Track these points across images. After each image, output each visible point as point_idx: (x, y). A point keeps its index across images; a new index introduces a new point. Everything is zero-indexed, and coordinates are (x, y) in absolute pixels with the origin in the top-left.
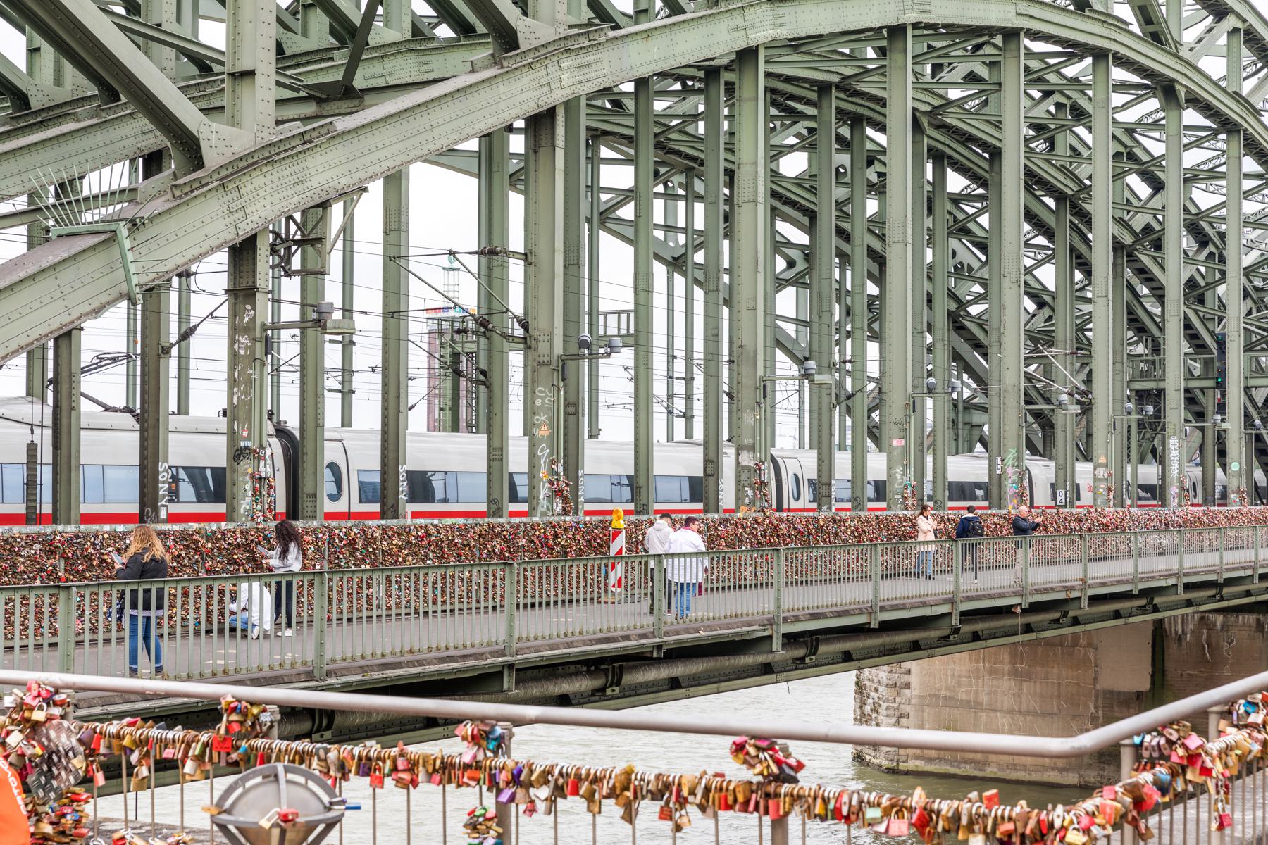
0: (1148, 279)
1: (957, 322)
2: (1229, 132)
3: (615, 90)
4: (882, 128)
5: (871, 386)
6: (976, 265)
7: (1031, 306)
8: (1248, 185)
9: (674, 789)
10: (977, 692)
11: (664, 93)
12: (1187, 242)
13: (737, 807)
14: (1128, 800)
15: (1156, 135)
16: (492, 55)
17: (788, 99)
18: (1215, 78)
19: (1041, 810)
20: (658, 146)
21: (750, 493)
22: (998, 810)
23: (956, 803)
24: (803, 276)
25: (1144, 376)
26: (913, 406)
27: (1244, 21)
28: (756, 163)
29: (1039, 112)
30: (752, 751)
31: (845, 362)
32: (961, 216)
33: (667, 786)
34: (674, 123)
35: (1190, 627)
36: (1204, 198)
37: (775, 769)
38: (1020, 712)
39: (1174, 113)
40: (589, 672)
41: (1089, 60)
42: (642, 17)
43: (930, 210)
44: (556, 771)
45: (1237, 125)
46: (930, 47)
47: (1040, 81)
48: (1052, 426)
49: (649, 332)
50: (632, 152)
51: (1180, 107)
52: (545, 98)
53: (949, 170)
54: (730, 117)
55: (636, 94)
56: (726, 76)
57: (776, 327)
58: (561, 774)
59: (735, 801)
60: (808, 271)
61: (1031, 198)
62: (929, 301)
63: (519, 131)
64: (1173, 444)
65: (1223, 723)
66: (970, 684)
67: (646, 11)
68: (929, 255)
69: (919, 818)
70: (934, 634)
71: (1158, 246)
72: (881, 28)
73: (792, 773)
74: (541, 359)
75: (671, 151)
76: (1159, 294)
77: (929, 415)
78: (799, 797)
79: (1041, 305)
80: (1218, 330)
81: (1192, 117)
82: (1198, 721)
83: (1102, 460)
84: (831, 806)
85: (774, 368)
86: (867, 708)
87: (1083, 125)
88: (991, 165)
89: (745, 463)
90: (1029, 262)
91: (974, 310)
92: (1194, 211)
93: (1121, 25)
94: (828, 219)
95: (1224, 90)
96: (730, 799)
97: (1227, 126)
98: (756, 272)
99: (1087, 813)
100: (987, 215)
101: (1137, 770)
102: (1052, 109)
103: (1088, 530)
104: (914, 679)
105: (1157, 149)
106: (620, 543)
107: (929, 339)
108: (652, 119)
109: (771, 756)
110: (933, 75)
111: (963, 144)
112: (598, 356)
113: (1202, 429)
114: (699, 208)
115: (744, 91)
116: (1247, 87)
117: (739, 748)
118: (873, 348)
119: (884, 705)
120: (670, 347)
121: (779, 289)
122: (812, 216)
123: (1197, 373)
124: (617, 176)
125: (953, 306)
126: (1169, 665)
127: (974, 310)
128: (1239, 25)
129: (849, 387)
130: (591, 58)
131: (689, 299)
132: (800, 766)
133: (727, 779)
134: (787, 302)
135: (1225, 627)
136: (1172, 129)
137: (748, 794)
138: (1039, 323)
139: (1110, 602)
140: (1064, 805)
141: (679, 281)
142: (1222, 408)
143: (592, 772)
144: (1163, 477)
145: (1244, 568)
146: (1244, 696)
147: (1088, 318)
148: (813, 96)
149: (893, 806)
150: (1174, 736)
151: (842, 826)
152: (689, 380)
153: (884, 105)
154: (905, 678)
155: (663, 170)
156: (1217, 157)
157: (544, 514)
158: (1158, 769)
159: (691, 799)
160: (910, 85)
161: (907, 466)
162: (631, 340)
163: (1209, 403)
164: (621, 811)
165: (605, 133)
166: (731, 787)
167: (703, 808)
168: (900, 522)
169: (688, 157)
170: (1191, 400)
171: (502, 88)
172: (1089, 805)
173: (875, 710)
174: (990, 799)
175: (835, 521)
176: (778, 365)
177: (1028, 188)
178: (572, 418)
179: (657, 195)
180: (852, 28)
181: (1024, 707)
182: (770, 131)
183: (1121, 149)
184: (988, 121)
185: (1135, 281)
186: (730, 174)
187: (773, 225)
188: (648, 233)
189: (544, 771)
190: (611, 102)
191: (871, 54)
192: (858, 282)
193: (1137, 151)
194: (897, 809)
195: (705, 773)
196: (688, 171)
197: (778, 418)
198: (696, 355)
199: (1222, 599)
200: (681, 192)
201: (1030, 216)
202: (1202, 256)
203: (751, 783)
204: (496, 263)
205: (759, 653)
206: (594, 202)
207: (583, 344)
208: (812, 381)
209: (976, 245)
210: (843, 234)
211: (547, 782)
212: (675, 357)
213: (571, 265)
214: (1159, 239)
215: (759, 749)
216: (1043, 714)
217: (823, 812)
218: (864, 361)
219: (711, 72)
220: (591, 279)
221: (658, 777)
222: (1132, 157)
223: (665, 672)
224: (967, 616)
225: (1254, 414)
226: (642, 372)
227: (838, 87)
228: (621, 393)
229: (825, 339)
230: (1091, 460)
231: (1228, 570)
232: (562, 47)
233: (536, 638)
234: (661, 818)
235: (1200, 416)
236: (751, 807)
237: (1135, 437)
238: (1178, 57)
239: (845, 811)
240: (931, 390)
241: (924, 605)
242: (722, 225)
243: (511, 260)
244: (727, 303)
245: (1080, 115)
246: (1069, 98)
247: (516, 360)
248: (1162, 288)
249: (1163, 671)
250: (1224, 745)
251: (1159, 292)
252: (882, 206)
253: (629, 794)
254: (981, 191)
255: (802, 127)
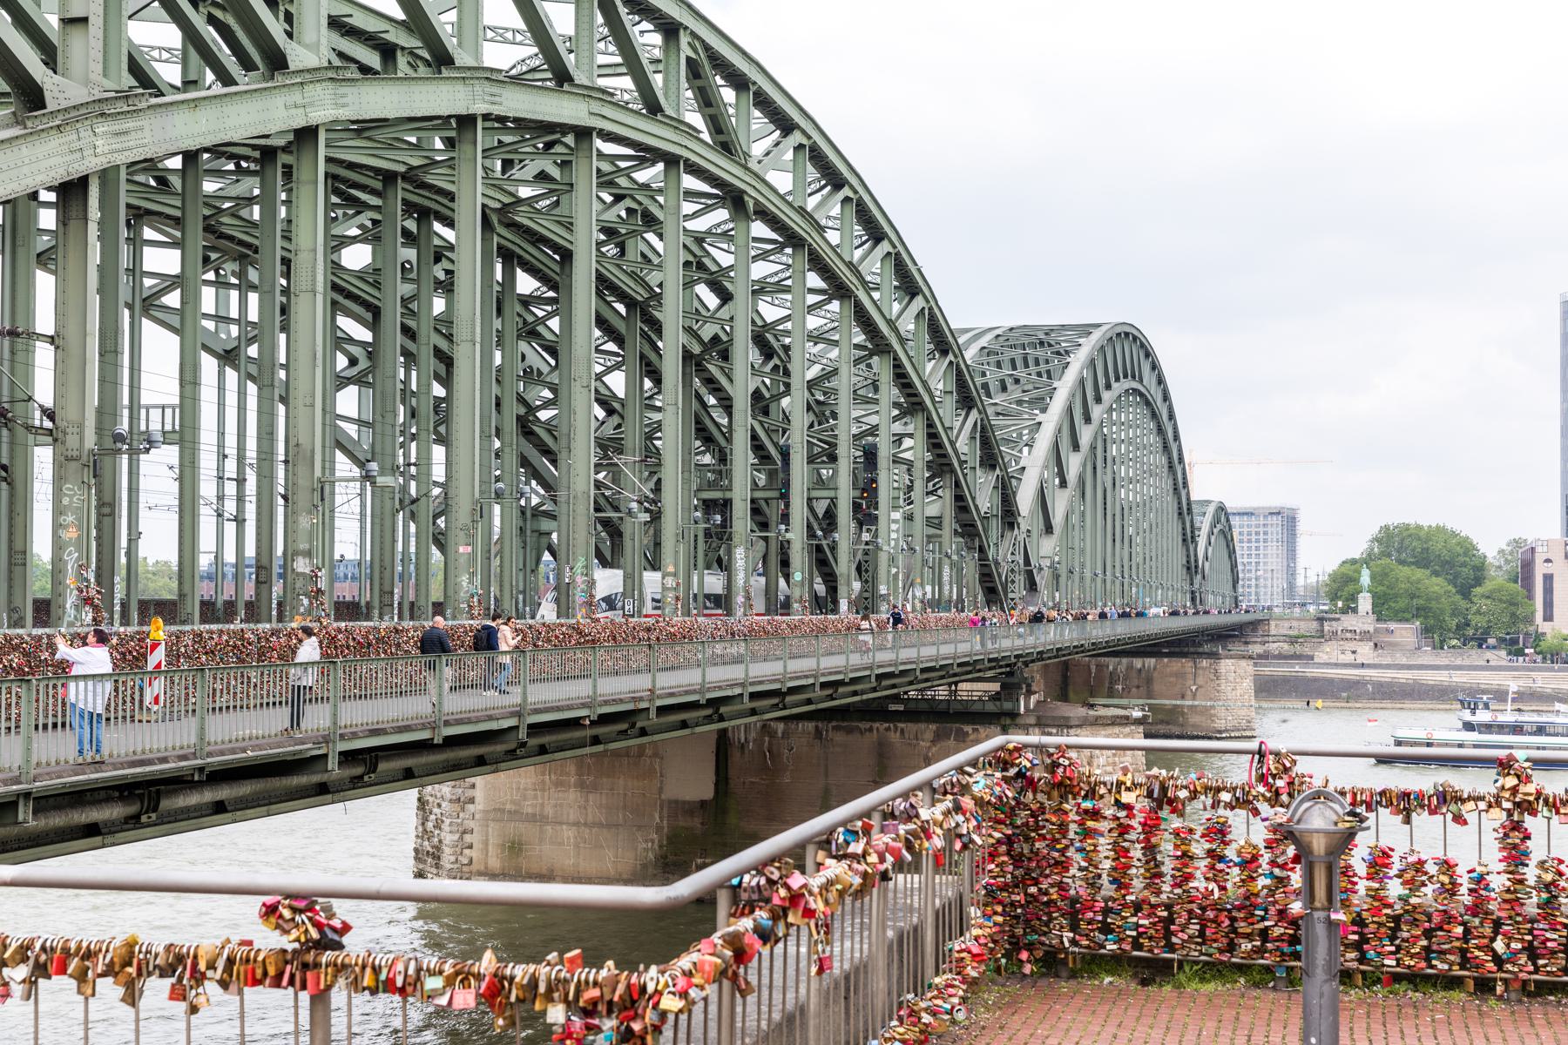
0: (716, 389)
1: (526, 426)
2: (794, 247)
3: (160, 166)
4: (450, 223)
5: (436, 491)
6: (545, 369)
7: (600, 413)
8: (812, 299)
9: (189, 962)
10: (542, 805)
11: (218, 173)
12: (754, 355)
13: (268, 982)
14: (729, 953)
15: (725, 246)
16: (14, 113)
17: (351, 187)
18: (782, 192)
19: (631, 972)
20: (208, 229)
21: (306, 602)
22: (582, 974)
23: (532, 968)
24: (366, 375)
25: (711, 485)
26: (481, 512)
27: (809, 138)
28: (315, 250)
29: (610, 216)
30: (287, 914)
31: (409, 465)
32: (530, 319)
33: (180, 959)
34: (227, 205)
35: (753, 735)
36: (770, 311)
37: (315, 934)
38: (585, 824)
39: (742, 225)
40: (122, 798)
41: (660, 166)
42: (192, 87)
43: (499, 312)
44: (38, 946)
45: (802, 239)
46: (500, 141)
47: (611, 184)
48: (620, 535)
49: (195, 429)
50: (178, 234)
51: (748, 219)
52: (76, 166)
53: (519, 271)
54: (288, 202)
55: (183, 172)
56: (284, 158)
57: (336, 426)
58: (43, 948)
59: (265, 974)
60: (371, 370)
61: (601, 303)
62: (498, 405)
63: (47, 205)
64: (739, 554)
65: (821, 855)
66: (535, 797)
67: (195, 82)
68: (498, 358)
69: (488, 988)
70: (500, 748)
71: (725, 356)
72: (450, 117)
73: (336, 937)
74: (69, 453)
75: (222, 236)
76: (727, 405)
77: (497, 521)
78: (344, 966)
79: (610, 412)
80: (782, 442)
81: (759, 229)
82: (796, 857)
83: (671, 569)
84: (383, 977)
85: (333, 470)
86: (430, 825)
87: (654, 232)
88: (562, 268)
89: (300, 570)
90: (599, 369)
91: (544, 415)
92: (760, 323)
93: (692, 132)
94: (393, 316)
95: (790, 204)
96: (259, 972)
97: (793, 240)
98: (314, 366)
99: (684, 973)
100: (557, 318)
101: (733, 915)
102: (623, 214)
103: (653, 640)
104: (478, 794)
105: (726, 260)
106: (159, 655)
107: (497, 444)
108: (201, 200)
109: (310, 919)
110: (504, 171)
111: (533, 244)
112: (139, 452)
113: (766, 539)
114: (253, 298)
115: (302, 173)
116: (811, 203)
117: (270, 911)
118: (439, 452)
119: (447, 821)
120: (221, 445)
121: (339, 387)
122: (376, 312)
123: (761, 483)
124: (162, 260)
125: (522, 411)
126: (732, 772)
127: (544, 415)
128: (805, 141)
129: (413, 492)
130: (129, 124)
131: (242, 394)
132: (347, 927)
133: (256, 947)
134: (348, 401)
135: (786, 734)
136: (740, 240)
137: (281, 965)
138: (608, 430)
139: (679, 712)
140: (657, 964)
141: (231, 376)
142: (785, 518)
143: (84, 945)
144: (729, 586)
145: (806, 677)
146: (843, 823)
147: (659, 426)
148: (378, 185)
149: (457, 974)
150: (776, 876)
151: (397, 998)
152: (241, 481)
153: (453, 200)
154: (469, 793)
155: (213, 256)
156: (782, 271)
157: (71, 624)
158: (758, 913)
159: (210, 974)
160: (479, 181)
161: (472, 575)
162: (177, 436)
163: (773, 513)
164: (121, 991)
165: (149, 212)
166: (260, 958)
167: (224, 984)
168: (466, 632)
169: (241, 243)
170: (756, 511)
171: (25, 151)
172: (685, 962)
173: (438, 826)
174: (572, 961)
175: (397, 631)
176: (338, 466)
177: (599, 294)
178: (107, 520)
179: (207, 283)
180: (420, 115)
181: (590, 819)
182: (330, 221)
183: (691, 259)
184: (559, 222)
185: (703, 391)
186: (286, 262)
187: (333, 320)
188: (196, 323)
189: (21, 946)
190: (156, 178)
191: (439, 145)
192: (424, 381)
193: (706, 261)
194: (463, 977)
195: (228, 941)
196: (242, 259)
197: (337, 523)
198: (248, 454)
199: (785, 708)
200: (234, 281)
201: (601, 322)
202: (768, 368)
203: (284, 951)
204: (20, 347)
205: (314, 773)
206: (136, 286)
207: (119, 438)
208: (373, 484)
209: (546, 348)
210: (407, 331)
211: (25, 959)
212: (225, 456)
213: (109, 351)
214: (727, 350)
215: (294, 910)
216: (609, 826)
217: (372, 984)
218: (429, 464)
219: (268, 154)
220: (132, 369)
221: (169, 948)
222: (701, 266)
223: (209, 796)
224: (535, 729)
225: (816, 526)
226: (188, 471)
227: (405, 177)
228: (166, 493)
229: (388, 440)
230: (659, 569)
231: (791, 679)
232: (97, 110)
233: (58, 763)
234: (171, 998)
235: (764, 526)
236: (285, 982)
237: (701, 546)
238: (747, 169)
239: (399, 982)
240: (499, 495)
241: (490, 718)
242: (278, 318)
243: (38, 344)
244: (284, 400)
245: (650, 221)
246: (640, 204)
247: (43, 458)
248: (729, 399)
249: (727, 779)
250: (824, 880)
251: (727, 403)
252: (450, 304)
253: (132, 970)
254: (551, 294)
255: (365, 219)
